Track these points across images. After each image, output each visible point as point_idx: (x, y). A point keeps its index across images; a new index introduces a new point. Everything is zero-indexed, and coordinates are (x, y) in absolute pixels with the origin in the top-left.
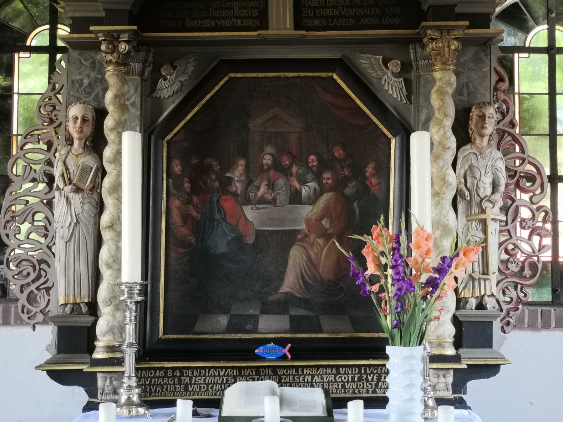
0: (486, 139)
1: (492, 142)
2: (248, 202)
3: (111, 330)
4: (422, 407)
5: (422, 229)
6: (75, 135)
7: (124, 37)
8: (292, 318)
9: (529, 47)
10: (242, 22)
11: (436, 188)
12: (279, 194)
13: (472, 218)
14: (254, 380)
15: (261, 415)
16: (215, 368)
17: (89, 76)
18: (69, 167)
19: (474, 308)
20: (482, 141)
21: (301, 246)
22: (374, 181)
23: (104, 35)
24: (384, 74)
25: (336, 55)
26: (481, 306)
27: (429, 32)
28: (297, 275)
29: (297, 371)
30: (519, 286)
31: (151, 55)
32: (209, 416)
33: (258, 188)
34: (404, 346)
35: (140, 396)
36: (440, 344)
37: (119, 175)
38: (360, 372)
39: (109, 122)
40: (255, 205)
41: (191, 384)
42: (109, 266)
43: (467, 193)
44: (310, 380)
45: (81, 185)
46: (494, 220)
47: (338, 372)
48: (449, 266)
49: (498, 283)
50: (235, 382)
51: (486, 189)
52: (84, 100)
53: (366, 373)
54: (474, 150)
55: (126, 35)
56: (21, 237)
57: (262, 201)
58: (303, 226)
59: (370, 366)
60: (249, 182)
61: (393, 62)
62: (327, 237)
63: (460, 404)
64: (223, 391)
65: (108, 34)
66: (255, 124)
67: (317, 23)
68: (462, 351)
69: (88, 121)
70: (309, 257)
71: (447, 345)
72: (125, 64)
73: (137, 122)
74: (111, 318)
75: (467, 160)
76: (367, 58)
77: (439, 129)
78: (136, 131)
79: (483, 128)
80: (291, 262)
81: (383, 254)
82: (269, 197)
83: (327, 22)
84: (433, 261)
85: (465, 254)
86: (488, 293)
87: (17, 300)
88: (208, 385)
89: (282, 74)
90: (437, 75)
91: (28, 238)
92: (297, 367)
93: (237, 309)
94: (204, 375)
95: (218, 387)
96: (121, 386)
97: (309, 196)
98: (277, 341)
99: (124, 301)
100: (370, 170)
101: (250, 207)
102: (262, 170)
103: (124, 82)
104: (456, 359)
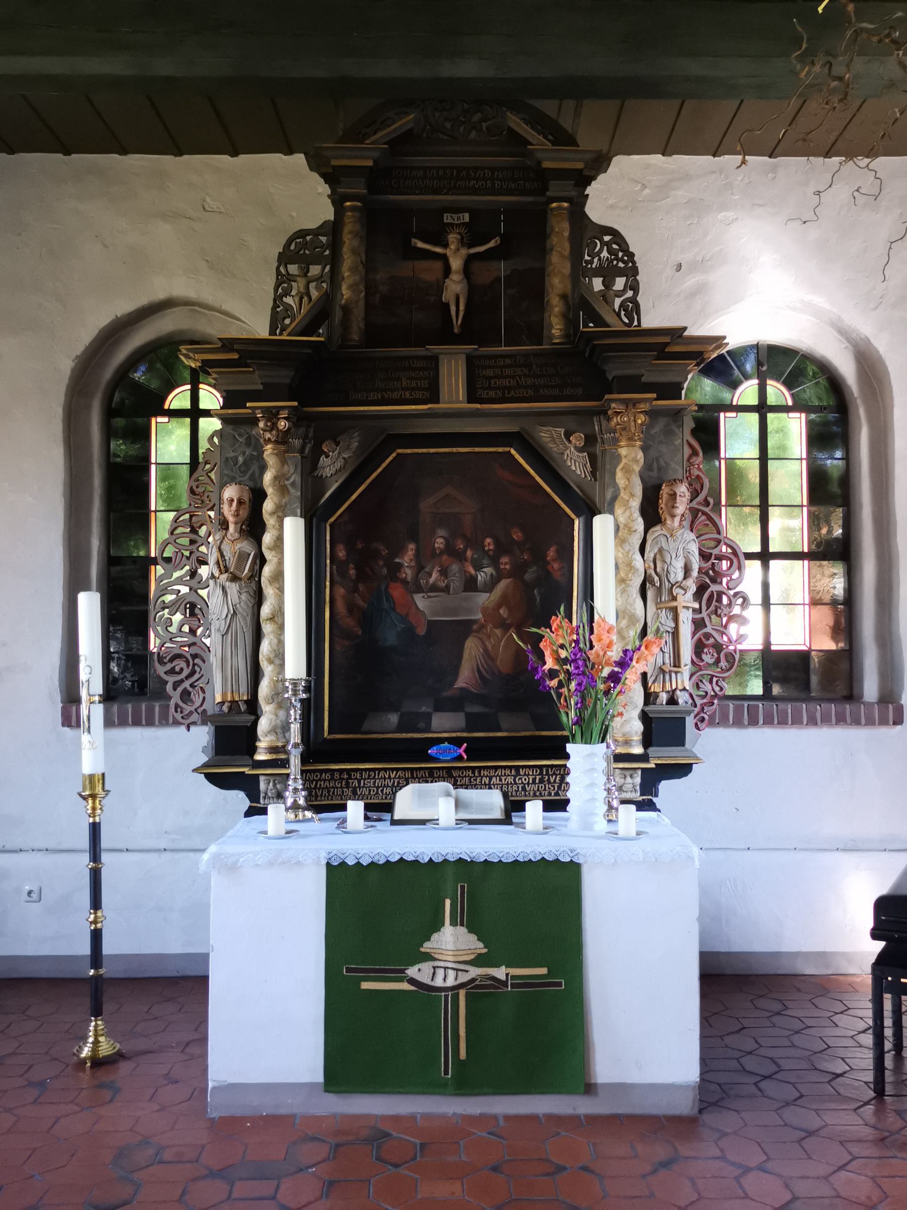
0: (677, 520)
1: (684, 523)
2: (419, 589)
3: (273, 730)
4: (606, 808)
5: (603, 620)
6: (231, 519)
7: (284, 414)
8: (468, 716)
9: (737, 406)
10: (411, 395)
11: (622, 574)
12: (452, 580)
13: (662, 605)
14: (427, 782)
15: (436, 817)
16: (385, 770)
17: (244, 454)
18: (225, 554)
19: (664, 703)
20: (673, 522)
21: (480, 638)
22: (556, 566)
23: (262, 412)
24: (567, 448)
25: (514, 429)
26: (672, 701)
27: (613, 405)
28: (473, 669)
29: (473, 773)
30: (715, 680)
31: (312, 430)
32: (380, 820)
33: (430, 575)
34: (586, 743)
35: (307, 799)
36: (627, 743)
37: (281, 563)
38: (541, 773)
39: (268, 506)
40: (426, 593)
41: (359, 787)
42: (270, 661)
43: (656, 578)
44: (487, 782)
45: (238, 573)
46: (687, 608)
47: (518, 774)
48: (631, 660)
49: (691, 676)
50: (407, 784)
51: (677, 574)
52: (239, 479)
53: (547, 774)
54: (665, 532)
55: (287, 412)
56: (173, 629)
57: (434, 588)
58: (479, 616)
59: (552, 766)
60: (420, 568)
61: (577, 434)
62: (505, 626)
63: (646, 805)
64: (394, 794)
65: (265, 410)
66: (426, 505)
67: (492, 394)
68: (652, 751)
69: (245, 503)
70: (486, 650)
71: (634, 743)
72: (284, 443)
73: (298, 504)
74: (273, 717)
75: (657, 543)
76: (548, 431)
77: (625, 510)
78: (296, 516)
79: (673, 507)
80: (466, 655)
81: (562, 646)
82: (442, 584)
83: (504, 394)
84: (615, 654)
85: (646, 647)
86: (680, 687)
87: (170, 698)
88: (378, 788)
89: (454, 450)
90: (623, 451)
91: (180, 631)
92: (473, 769)
93: (409, 706)
94: (374, 778)
95: (389, 790)
96: (286, 787)
97: (485, 582)
98: (450, 740)
99: (288, 698)
100: (551, 553)
101: (422, 595)
102: (434, 555)
103: (283, 461)
104: (644, 758)
